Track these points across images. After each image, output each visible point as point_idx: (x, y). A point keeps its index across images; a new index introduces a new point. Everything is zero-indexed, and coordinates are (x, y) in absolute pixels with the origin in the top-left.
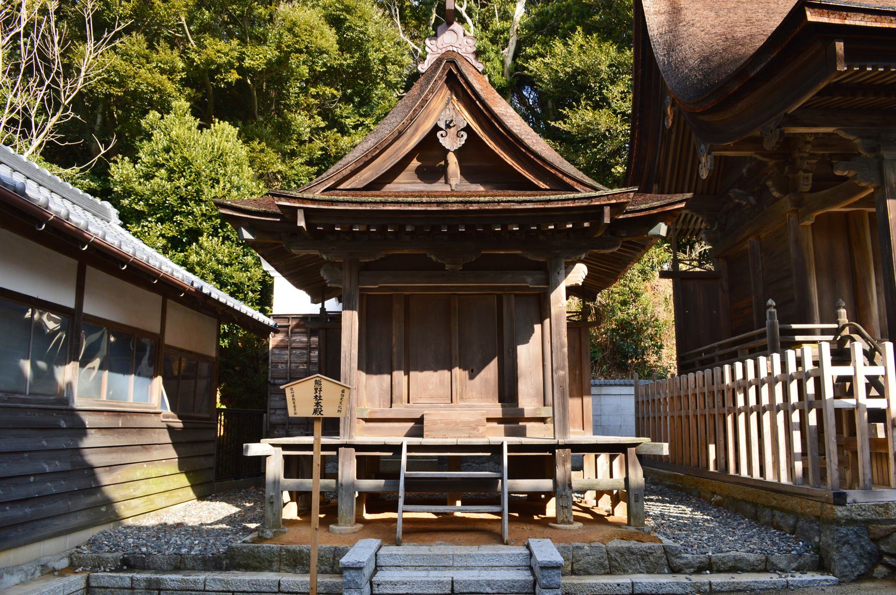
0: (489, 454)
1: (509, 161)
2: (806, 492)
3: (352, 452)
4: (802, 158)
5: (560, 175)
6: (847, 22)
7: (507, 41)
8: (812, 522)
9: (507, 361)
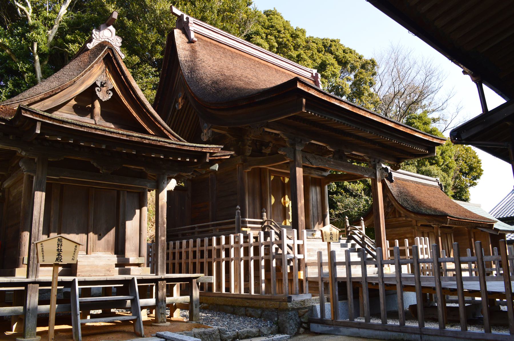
0: (122, 285)
1: (135, 114)
2: (270, 298)
3: (38, 287)
4: (248, 140)
5: (163, 129)
6: (309, 92)
7: (52, 26)
8: (273, 311)
9: (121, 230)
